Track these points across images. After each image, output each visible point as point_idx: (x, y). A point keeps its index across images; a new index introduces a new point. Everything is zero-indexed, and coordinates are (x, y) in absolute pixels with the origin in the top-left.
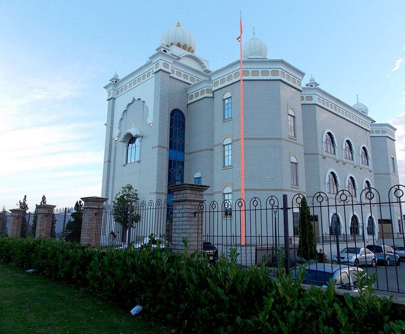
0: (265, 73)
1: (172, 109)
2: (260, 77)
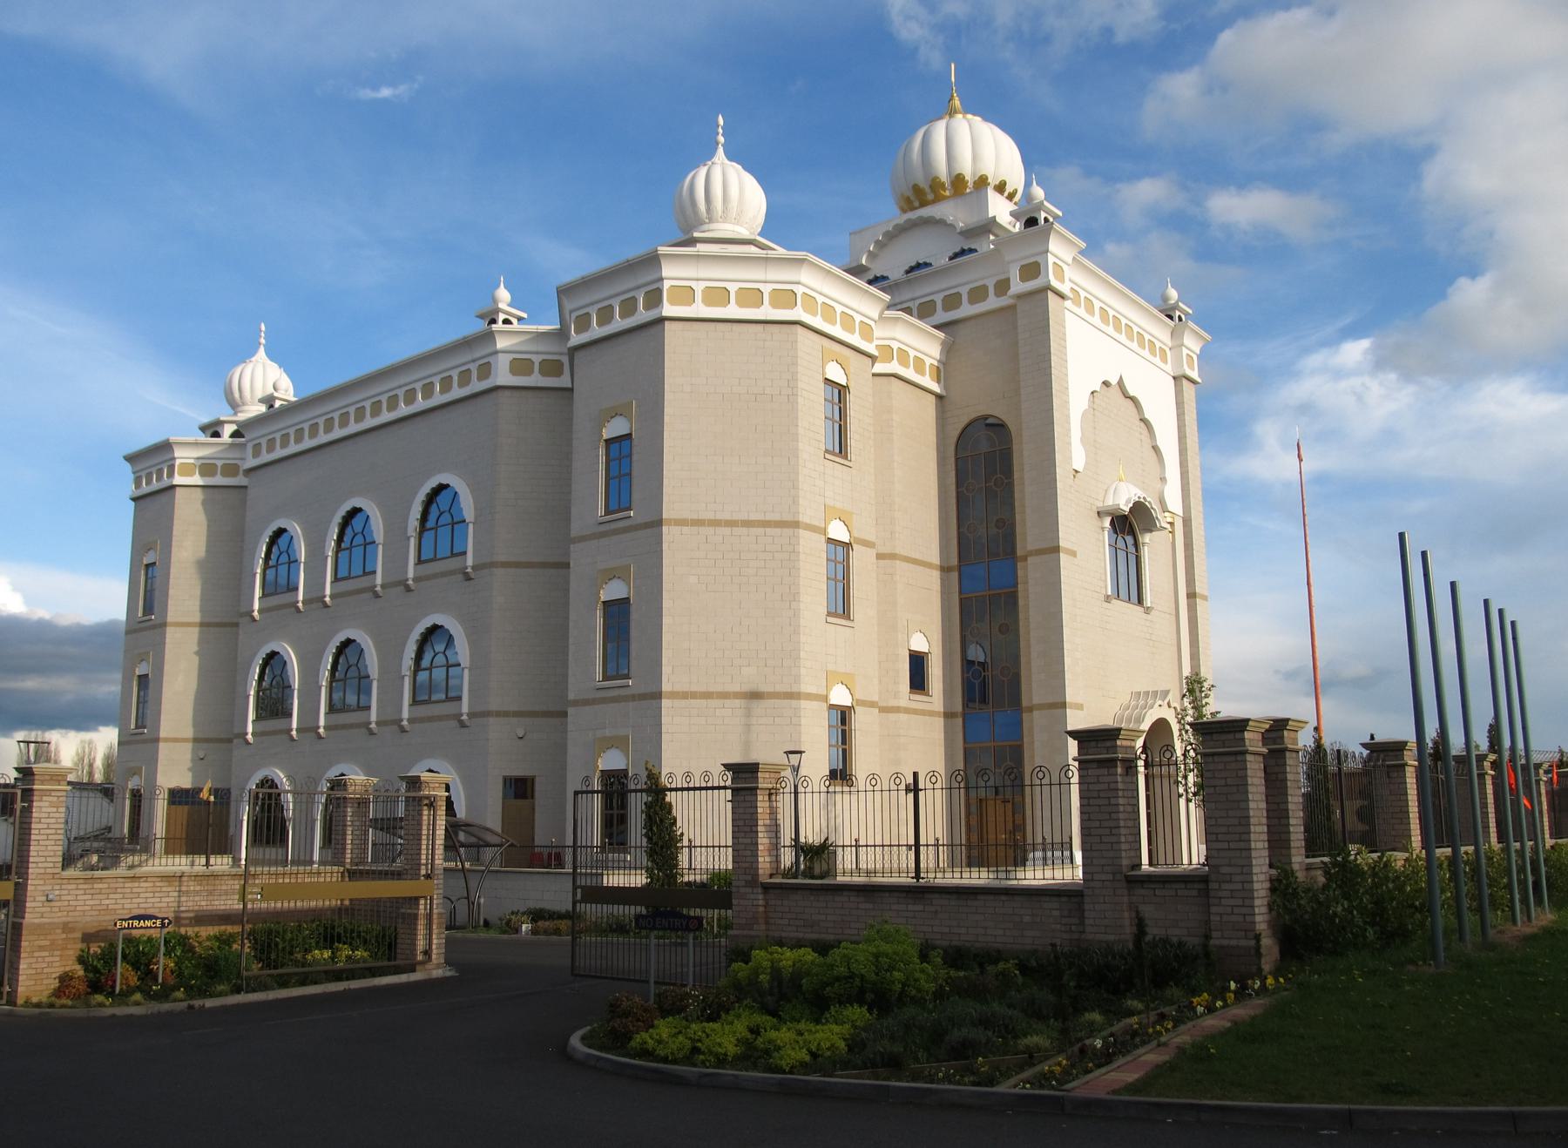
0: (752, 297)
1: (1000, 411)
2: (733, 311)
